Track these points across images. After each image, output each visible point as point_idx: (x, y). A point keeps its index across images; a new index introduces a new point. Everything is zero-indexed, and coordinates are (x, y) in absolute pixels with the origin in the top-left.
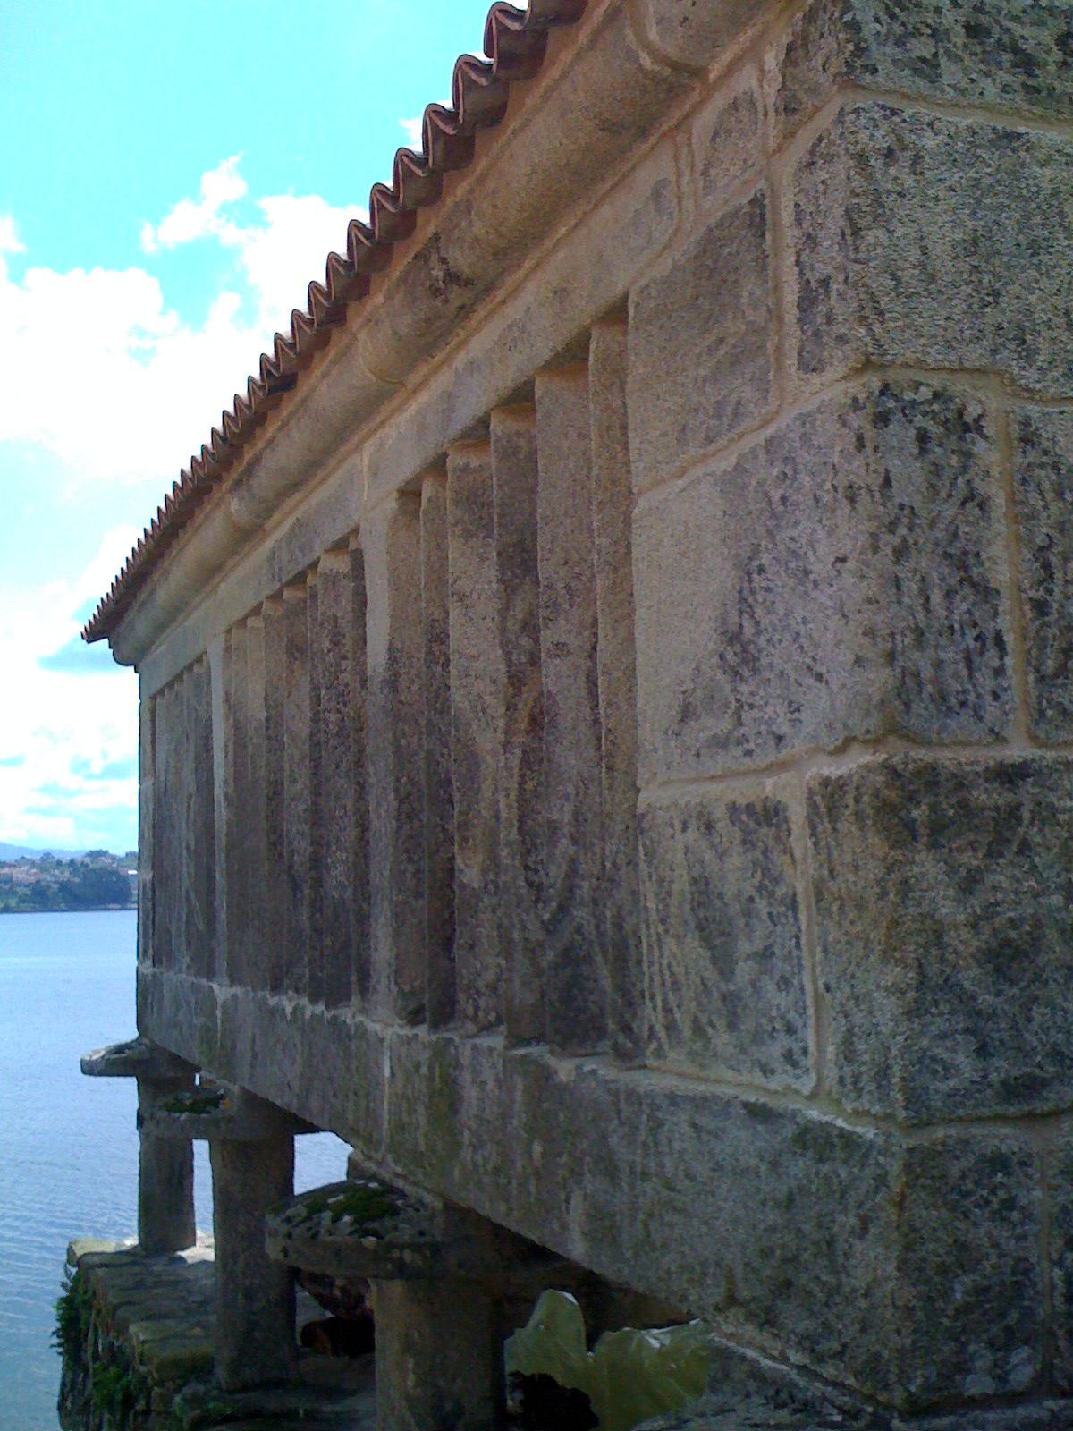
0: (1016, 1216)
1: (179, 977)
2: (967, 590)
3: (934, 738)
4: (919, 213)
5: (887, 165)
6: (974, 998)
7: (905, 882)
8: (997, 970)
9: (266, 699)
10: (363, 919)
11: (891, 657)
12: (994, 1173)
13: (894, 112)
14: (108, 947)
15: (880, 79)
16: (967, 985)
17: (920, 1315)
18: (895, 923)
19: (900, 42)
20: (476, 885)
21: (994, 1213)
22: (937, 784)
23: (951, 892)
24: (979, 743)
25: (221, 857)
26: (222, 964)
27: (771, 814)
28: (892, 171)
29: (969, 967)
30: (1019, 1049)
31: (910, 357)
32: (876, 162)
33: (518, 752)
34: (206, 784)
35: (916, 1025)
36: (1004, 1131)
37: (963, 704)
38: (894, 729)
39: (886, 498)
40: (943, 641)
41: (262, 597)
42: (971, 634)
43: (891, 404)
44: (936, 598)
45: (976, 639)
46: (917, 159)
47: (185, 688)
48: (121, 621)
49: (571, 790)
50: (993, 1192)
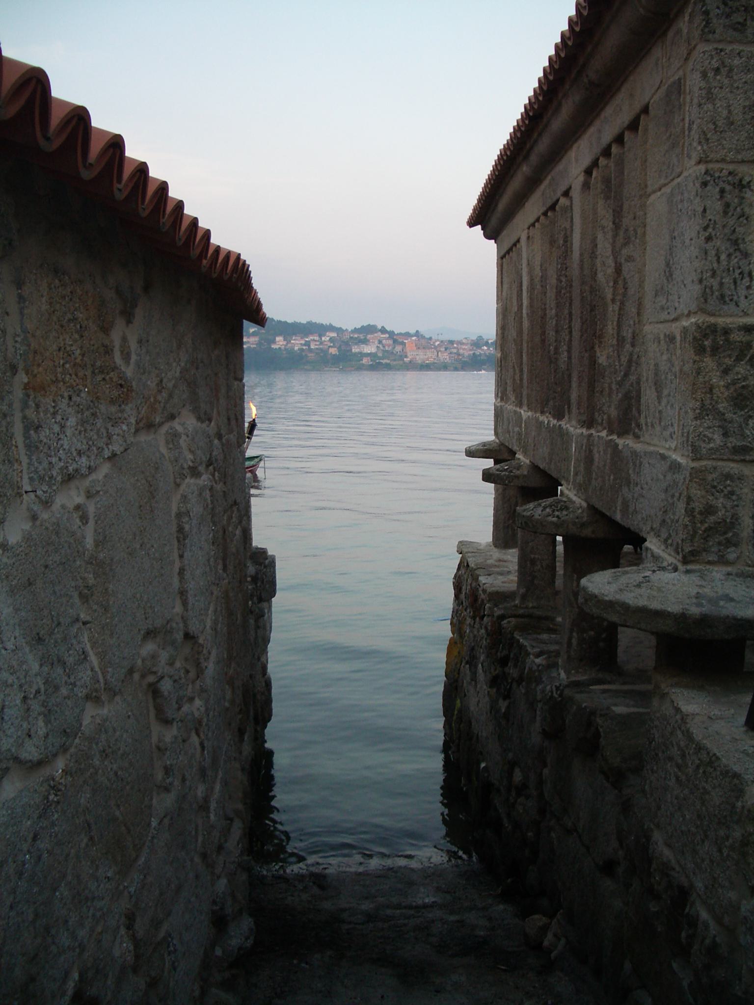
0: (734, 497)
1: (510, 407)
2: (738, 254)
3: (717, 313)
4: (729, 95)
5: (715, 75)
6: (724, 414)
7: (700, 368)
8: (735, 404)
9: (541, 266)
10: (570, 376)
11: (701, 281)
12: (726, 480)
13: (721, 50)
14: (482, 387)
15: (717, 36)
16: (721, 409)
17: (690, 528)
18: (694, 384)
19: (728, 16)
20: (604, 364)
21: (725, 495)
22: (716, 331)
23: (718, 374)
24: (737, 315)
25: (525, 345)
26: (525, 401)
27: (671, 339)
28: (718, 77)
29: (723, 402)
30: (742, 435)
31: (719, 156)
32: (711, 74)
33: (618, 303)
34: (520, 306)
35: (698, 422)
36: (732, 465)
37: (731, 300)
38: (703, 311)
39: (704, 217)
40: (724, 275)
41: (540, 214)
42: (738, 271)
43: (709, 178)
44: (723, 257)
45: (740, 274)
46: (731, 70)
47: (513, 254)
48: (489, 215)
49: (632, 323)
50: (725, 487)
